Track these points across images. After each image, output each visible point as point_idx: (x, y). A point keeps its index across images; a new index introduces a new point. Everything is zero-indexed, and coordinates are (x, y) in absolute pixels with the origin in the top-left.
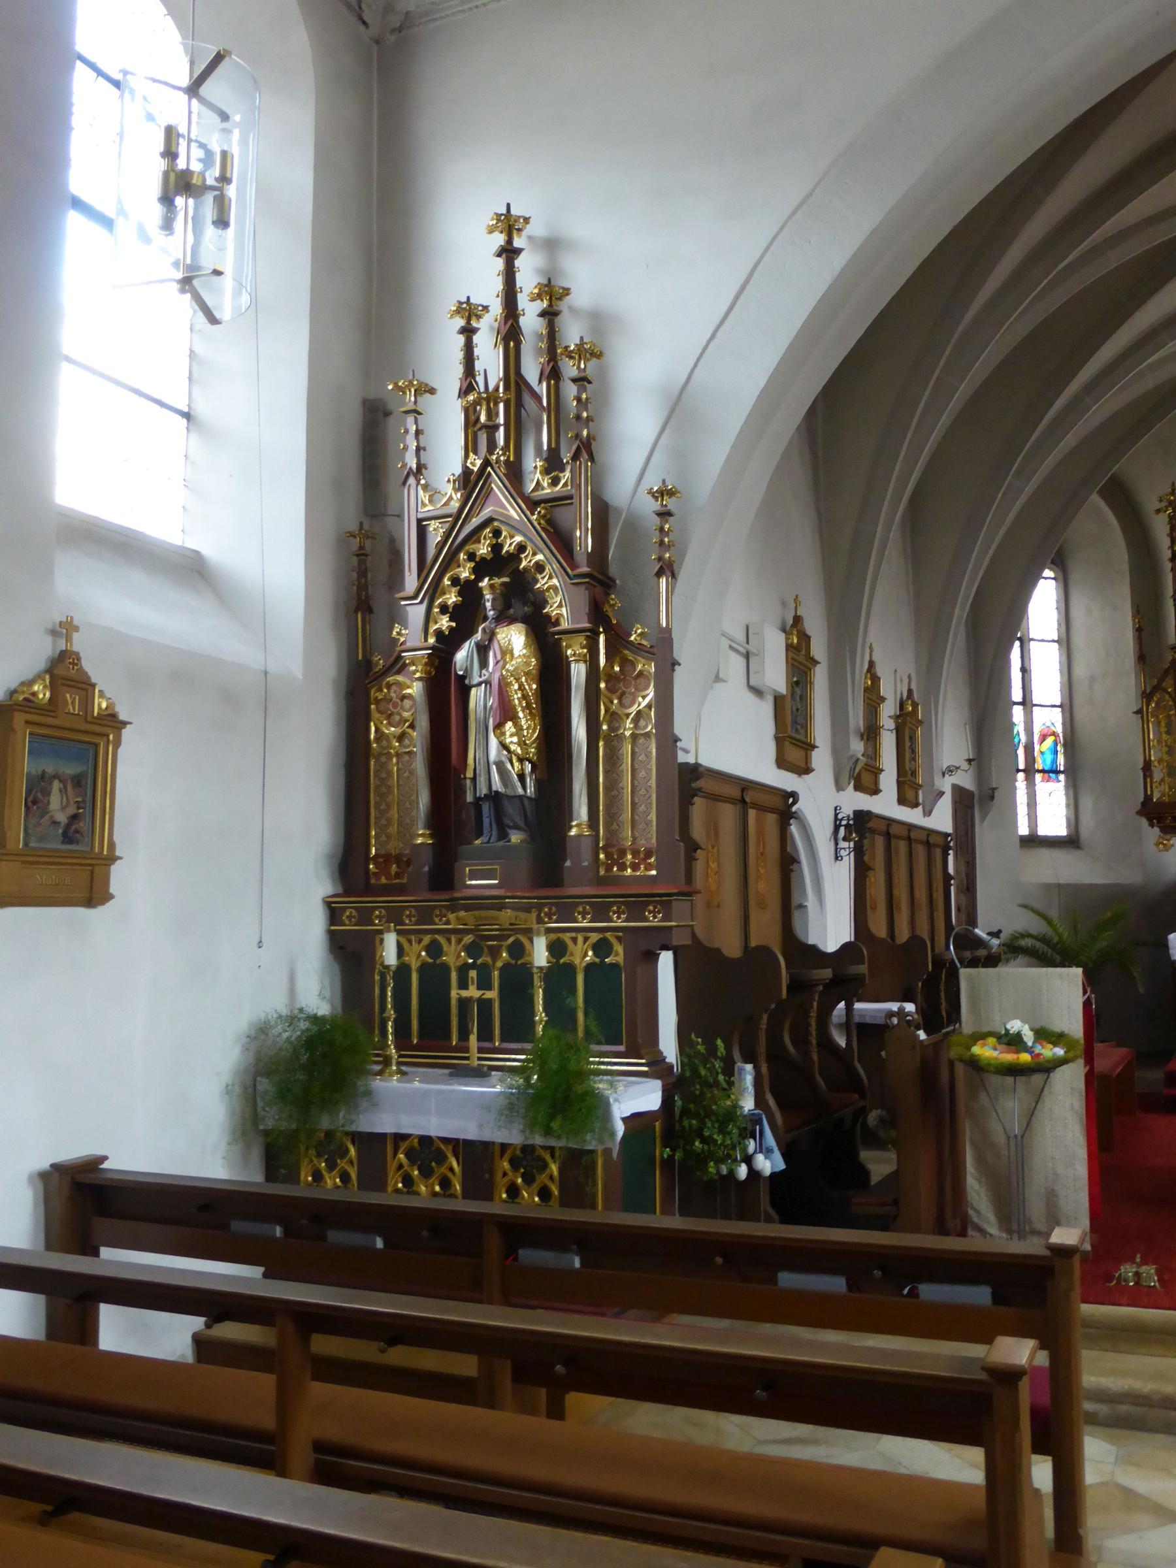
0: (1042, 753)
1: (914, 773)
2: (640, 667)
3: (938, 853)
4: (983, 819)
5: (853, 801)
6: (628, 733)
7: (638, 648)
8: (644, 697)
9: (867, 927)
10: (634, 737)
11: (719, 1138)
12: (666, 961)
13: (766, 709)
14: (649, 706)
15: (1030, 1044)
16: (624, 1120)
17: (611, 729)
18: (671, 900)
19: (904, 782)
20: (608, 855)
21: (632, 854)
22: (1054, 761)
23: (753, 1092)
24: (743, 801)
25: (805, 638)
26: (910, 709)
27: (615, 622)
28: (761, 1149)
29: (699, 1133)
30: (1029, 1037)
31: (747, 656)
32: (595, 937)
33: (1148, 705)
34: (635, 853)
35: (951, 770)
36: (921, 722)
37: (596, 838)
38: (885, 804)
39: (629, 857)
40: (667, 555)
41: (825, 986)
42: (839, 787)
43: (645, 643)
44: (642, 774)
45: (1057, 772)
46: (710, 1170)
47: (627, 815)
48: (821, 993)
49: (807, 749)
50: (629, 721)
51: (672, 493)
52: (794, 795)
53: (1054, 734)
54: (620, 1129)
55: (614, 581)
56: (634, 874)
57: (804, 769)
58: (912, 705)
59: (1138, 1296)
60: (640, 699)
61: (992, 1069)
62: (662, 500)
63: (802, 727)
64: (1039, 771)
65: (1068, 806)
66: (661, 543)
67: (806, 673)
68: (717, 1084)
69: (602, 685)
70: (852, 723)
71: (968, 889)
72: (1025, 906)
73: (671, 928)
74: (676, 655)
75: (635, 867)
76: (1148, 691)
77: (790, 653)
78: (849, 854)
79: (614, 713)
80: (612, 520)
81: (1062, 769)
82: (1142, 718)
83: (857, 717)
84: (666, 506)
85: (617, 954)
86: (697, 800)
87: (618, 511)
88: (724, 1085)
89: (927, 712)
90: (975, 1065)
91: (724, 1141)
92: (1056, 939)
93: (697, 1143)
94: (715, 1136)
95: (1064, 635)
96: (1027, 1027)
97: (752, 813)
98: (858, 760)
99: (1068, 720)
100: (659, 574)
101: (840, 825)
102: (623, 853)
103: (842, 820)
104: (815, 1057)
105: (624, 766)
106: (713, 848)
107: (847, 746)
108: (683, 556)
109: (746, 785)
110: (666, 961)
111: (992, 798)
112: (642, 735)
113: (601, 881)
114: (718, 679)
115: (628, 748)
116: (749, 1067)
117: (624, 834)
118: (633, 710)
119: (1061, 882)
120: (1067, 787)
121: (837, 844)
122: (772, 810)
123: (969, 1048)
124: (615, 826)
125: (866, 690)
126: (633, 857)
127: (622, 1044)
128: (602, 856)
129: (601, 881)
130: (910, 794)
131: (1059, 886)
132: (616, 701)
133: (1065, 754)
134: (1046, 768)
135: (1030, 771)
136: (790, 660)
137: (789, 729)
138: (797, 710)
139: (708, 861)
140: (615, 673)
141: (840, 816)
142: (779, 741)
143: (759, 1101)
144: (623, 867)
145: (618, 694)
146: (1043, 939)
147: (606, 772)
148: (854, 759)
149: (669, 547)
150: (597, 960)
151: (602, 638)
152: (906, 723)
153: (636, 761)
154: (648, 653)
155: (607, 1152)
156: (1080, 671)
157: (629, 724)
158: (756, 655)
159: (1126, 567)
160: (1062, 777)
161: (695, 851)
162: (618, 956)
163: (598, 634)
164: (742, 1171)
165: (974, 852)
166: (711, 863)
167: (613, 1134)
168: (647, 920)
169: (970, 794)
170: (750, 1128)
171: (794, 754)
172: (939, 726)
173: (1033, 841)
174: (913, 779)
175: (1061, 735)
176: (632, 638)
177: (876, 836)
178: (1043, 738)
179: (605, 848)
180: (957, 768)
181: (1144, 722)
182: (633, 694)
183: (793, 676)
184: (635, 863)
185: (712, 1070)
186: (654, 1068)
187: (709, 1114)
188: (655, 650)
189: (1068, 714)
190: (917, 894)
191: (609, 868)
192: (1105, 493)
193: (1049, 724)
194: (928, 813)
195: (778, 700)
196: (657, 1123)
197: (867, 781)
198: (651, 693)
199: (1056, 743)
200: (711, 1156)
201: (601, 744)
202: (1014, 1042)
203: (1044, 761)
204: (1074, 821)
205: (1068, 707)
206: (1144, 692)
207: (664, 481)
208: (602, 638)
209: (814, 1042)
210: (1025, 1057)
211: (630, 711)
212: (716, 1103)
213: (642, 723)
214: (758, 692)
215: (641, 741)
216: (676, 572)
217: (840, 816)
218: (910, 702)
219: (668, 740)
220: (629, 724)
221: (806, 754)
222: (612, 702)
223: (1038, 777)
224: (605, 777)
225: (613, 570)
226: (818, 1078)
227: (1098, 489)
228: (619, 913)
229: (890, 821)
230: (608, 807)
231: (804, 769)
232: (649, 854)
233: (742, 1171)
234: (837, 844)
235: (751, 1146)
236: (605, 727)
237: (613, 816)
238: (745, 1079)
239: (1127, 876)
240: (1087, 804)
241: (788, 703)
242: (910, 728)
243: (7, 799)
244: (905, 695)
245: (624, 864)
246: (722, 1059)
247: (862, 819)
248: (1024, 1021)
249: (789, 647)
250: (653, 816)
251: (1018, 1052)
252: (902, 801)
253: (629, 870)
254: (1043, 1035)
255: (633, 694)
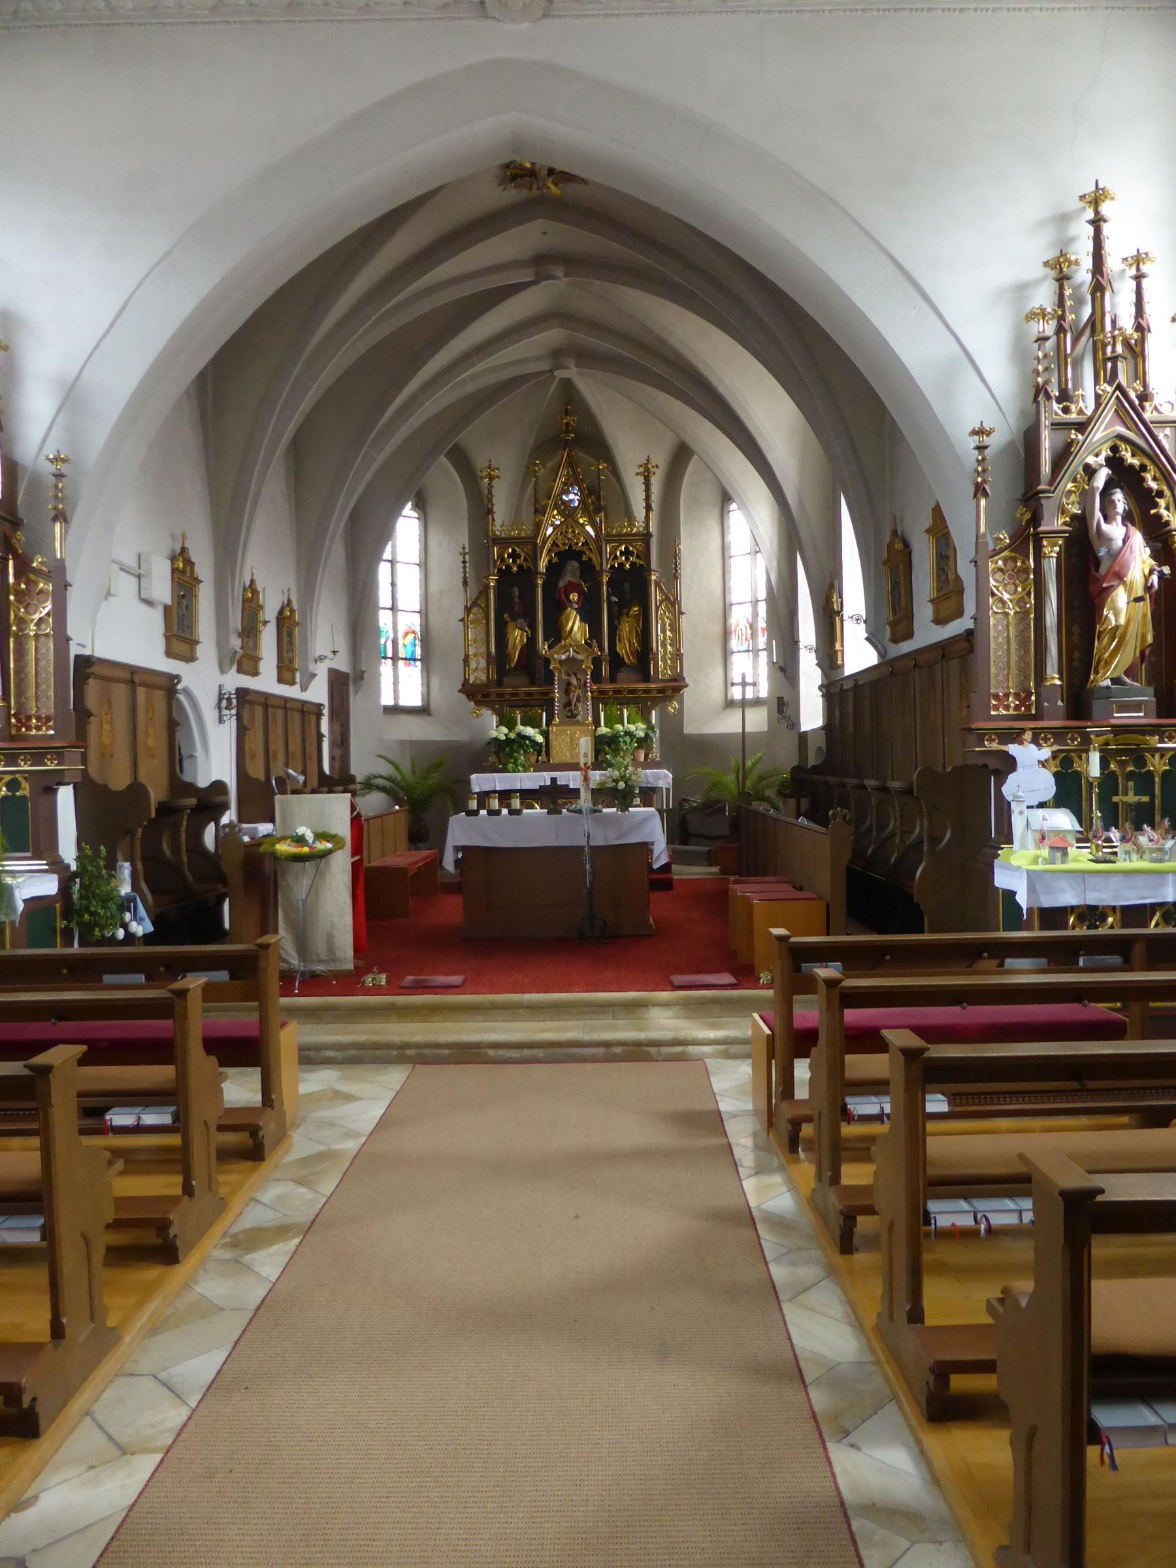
0: (405, 646)
1: (291, 661)
2: (41, 585)
3: (313, 718)
4: (356, 692)
5: (234, 681)
6: (32, 633)
7: (38, 572)
8: (44, 608)
9: (246, 773)
10: (37, 636)
11: (102, 912)
12: (65, 797)
13: (157, 616)
14: (48, 614)
15: (311, 841)
16: (24, 901)
17: (20, 629)
18: (63, 752)
19: (282, 667)
20: (18, 720)
21: (36, 719)
22: (413, 652)
23: (130, 881)
24: (132, 682)
25: (189, 563)
26: (289, 614)
27: (20, 552)
28: (135, 917)
29: (87, 909)
30: (310, 837)
31: (139, 577)
32: (7, 778)
33: (468, 616)
34: (38, 718)
35: (321, 658)
36: (297, 624)
37: (9, 707)
38: (266, 682)
39: (34, 721)
40: (61, 506)
41: (191, 809)
42: (223, 671)
43: (44, 569)
44: (43, 663)
45: (415, 660)
46: (96, 933)
47: (32, 692)
48: (189, 814)
49: (192, 644)
50: (32, 625)
51: (64, 461)
52: (178, 677)
53: (414, 632)
54: (20, 906)
55: (23, 520)
56: (38, 733)
57: (190, 658)
58: (290, 611)
59: (376, 990)
60: (41, 609)
61: (283, 857)
62: (57, 465)
63: (188, 628)
64: (402, 659)
65: (422, 684)
66: (56, 497)
67: (192, 589)
68: (100, 876)
69: (12, 598)
70: (232, 625)
71: (342, 743)
72: (380, 756)
73: (64, 770)
74: (69, 579)
75: (38, 728)
76: (469, 606)
77: (176, 575)
78: (230, 719)
79: (21, 618)
80: (20, 473)
81: (419, 658)
82: (464, 624)
83: (235, 620)
84: (59, 469)
85: (24, 789)
86: (90, 680)
87: (25, 468)
88: (106, 876)
89: (304, 616)
90: (274, 856)
91: (105, 913)
92: (399, 778)
93: (86, 916)
94: (99, 911)
95: (423, 561)
96: (309, 831)
97: (141, 692)
98: (236, 652)
99: (424, 621)
100: (55, 519)
101: (223, 698)
102: (29, 718)
103: (225, 693)
104: (185, 858)
105: (29, 657)
106: (106, 714)
107: (228, 642)
108: (75, 505)
109: (133, 670)
110: (65, 797)
111: (362, 678)
112: (43, 635)
113: (13, 738)
114: (109, 594)
115: (32, 645)
116: (127, 865)
117: (30, 705)
118: (36, 617)
119: (413, 739)
120: (422, 671)
121: (220, 712)
122: (160, 688)
123: (274, 845)
124: (23, 699)
125: (245, 601)
126: (37, 722)
127: (29, 851)
128: (13, 720)
129: (13, 738)
130: (287, 675)
131: (411, 742)
132: (22, 610)
133: (422, 647)
134: (408, 657)
135: (395, 658)
136: (176, 580)
137: (175, 628)
138: (184, 615)
139: (102, 724)
140: (23, 590)
141: (223, 692)
142: (168, 638)
143: (135, 886)
144: (29, 728)
145: (24, 605)
146: (389, 779)
147: (15, 661)
148: (233, 652)
149: (62, 500)
150: (10, 794)
151: (11, 563)
152: (285, 623)
153: (38, 653)
154: (47, 577)
155: (12, 923)
156: (433, 587)
157: (32, 627)
158: (146, 576)
159: (465, 514)
160: (419, 663)
161: (89, 717)
162: (25, 790)
163: (7, 560)
164: (121, 933)
165: (348, 716)
166: (105, 726)
167: (15, 909)
168: (46, 765)
169: (346, 675)
170: (126, 905)
171: (182, 648)
172: (313, 626)
173: (395, 710)
174: (291, 665)
175: (419, 633)
176: (34, 565)
177: (256, 706)
178: (406, 634)
179: (15, 715)
180: (326, 657)
181: (466, 627)
182: (36, 605)
183: (181, 591)
184: (18, 726)
185: (98, 867)
186: (54, 867)
187: (95, 895)
188: (51, 574)
189: (424, 617)
190: (292, 747)
191: (19, 729)
192: (449, 456)
193: (411, 625)
194: (304, 689)
195: (167, 609)
196: (57, 905)
197: (248, 663)
198: (49, 606)
199: (415, 638)
200: (96, 924)
201: (11, 640)
202: (300, 840)
203: (406, 652)
204: (427, 696)
205: (424, 613)
206: (466, 606)
207: (58, 451)
208: (11, 563)
209: (184, 849)
210: (306, 849)
211: (34, 617)
212: (99, 889)
213: (43, 626)
214: (149, 603)
215: (42, 639)
216: (68, 517)
217: (223, 692)
218: (288, 609)
219: (62, 640)
220: (32, 627)
221: (192, 647)
222: (19, 610)
223: (401, 663)
224: (15, 664)
225: (22, 512)
226: (187, 872)
227: (445, 452)
228: (25, 760)
229: (267, 696)
230: (17, 686)
231: (190, 658)
232: (48, 719)
233: (121, 933)
234: (220, 712)
235: (128, 916)
236: (14, 628)
237: (20, 693)
238: (124, 872)
239: (460, 735)
240: (435, 683)
241: (175, 611)
242: (288, 627)
243: (863, 991)
244: (286, 602)
245: (30, 726)
246: (105, 859)
247: (242, 693)
248: (308, 827)
249: (174, 570)
250: (51, 693)
251: (302, 847)
252: (280, 680)
253: (34, 731)
254: (320, 836)
255: (36, 605)
